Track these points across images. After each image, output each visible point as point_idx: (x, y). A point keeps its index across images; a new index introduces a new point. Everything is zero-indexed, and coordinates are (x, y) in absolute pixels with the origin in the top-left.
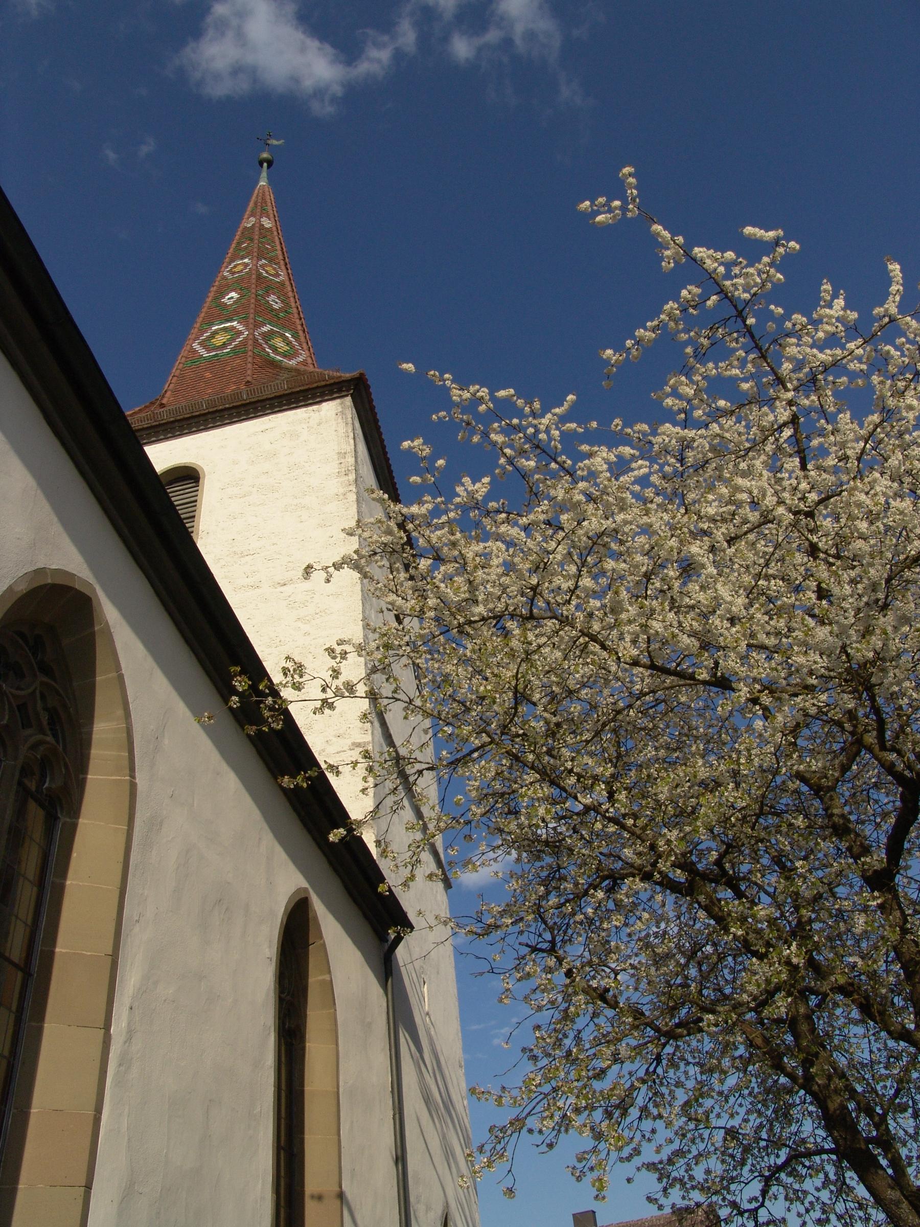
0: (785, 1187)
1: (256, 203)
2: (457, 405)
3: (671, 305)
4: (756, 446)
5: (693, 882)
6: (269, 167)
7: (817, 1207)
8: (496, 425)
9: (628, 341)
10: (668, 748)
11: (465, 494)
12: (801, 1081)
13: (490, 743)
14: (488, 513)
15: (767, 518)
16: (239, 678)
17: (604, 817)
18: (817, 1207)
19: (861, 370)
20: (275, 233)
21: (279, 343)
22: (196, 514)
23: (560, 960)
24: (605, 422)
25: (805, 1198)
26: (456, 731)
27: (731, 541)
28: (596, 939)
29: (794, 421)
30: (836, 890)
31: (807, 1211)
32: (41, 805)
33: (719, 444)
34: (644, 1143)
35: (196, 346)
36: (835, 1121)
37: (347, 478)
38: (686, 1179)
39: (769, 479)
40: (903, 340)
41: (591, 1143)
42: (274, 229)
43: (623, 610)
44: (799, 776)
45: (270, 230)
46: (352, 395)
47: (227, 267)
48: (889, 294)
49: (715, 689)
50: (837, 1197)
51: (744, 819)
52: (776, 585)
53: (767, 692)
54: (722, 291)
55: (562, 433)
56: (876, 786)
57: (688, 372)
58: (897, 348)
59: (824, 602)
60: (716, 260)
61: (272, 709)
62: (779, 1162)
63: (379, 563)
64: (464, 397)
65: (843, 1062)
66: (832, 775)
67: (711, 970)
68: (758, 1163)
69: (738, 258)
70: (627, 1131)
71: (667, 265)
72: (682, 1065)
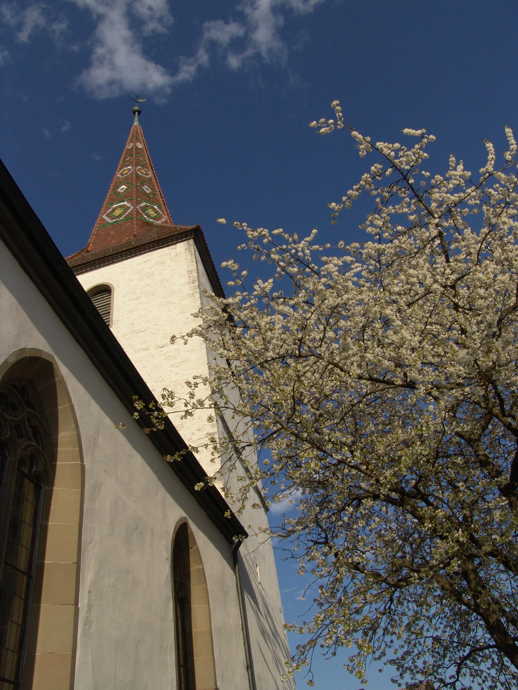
0: (470, 669)
1: (133, 135)
2: (251, 240)
3: (366, 176)
4: (420, 250)
5: (403, 498)
6: (139, 114)
7: (489, 679)
8: (274, 249)
9: (344, 198)
10: (384, 424)
11: (259, 289)
12: (473, 607)
13: (282, 428)
14: (273, 299)
15: (428, 291)
16: (138, 402)
17: (349, 465)
18: (489, 679)
19: (477, 204)
20: (145, 151)
21: (151, 212)
22: (111, 311)
23: (331, 548)
24: (335, 243)
25: (482, 674)
26: (262, 423)
27: (409, 305)
28: (350, 535)
29: (440, 235)
30: (485, 497)
31: (484, 682)
32: (31, 481)
33: (400, 251)
34: (387, 649)
35: (104, 217)
36: (494, 628)
37: (193, 285)
38: (413, 668)
39: (428, 269)
40: (498, 185)
41: (358, 651)
42: (144, 148)
43: (350, 349)
44: (458, 434)
45: (141, 149)
46: (193, 238)
47: (119, 172)
48: (488, 160)
49: (408, 389)
50: (500, 673)
51: (428, 461)
52: (435, 328)
53: (435, 388)
54: (394, 166)
55: (311, 251)
56: (503, 436)
57: (379, 212)
58: (495, 190)
59: (463, 336)
60: (390, 148)
61: (157, 418)
62: (465, 654)
63: (214, 332)
64: (255, 235)
65: (497, 595)
66: (476, 432)
67: (418, 547)
68: (453, 656)
69: (401, 146)
70: (377, 642)
71: (362, 154)
72: (405, 603)
